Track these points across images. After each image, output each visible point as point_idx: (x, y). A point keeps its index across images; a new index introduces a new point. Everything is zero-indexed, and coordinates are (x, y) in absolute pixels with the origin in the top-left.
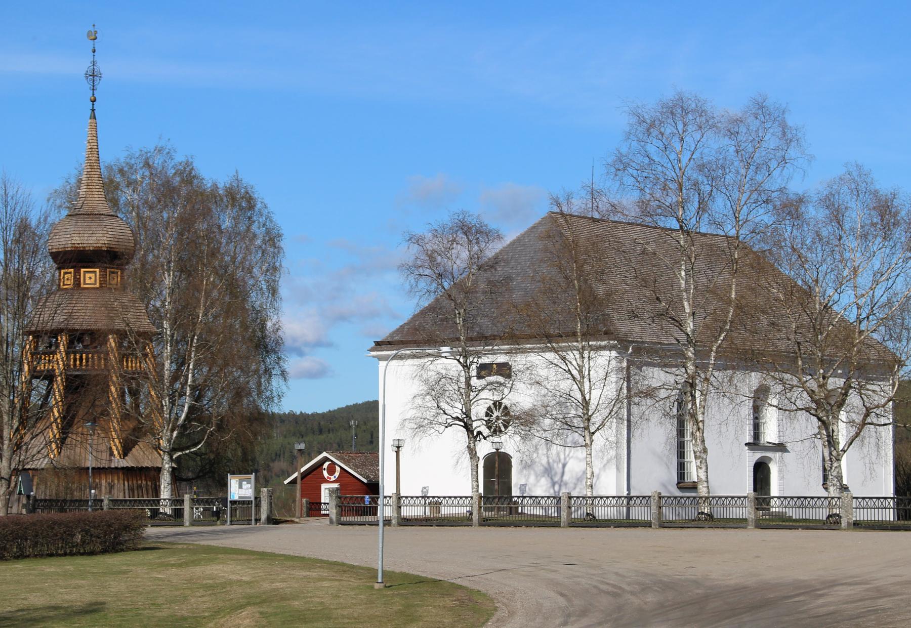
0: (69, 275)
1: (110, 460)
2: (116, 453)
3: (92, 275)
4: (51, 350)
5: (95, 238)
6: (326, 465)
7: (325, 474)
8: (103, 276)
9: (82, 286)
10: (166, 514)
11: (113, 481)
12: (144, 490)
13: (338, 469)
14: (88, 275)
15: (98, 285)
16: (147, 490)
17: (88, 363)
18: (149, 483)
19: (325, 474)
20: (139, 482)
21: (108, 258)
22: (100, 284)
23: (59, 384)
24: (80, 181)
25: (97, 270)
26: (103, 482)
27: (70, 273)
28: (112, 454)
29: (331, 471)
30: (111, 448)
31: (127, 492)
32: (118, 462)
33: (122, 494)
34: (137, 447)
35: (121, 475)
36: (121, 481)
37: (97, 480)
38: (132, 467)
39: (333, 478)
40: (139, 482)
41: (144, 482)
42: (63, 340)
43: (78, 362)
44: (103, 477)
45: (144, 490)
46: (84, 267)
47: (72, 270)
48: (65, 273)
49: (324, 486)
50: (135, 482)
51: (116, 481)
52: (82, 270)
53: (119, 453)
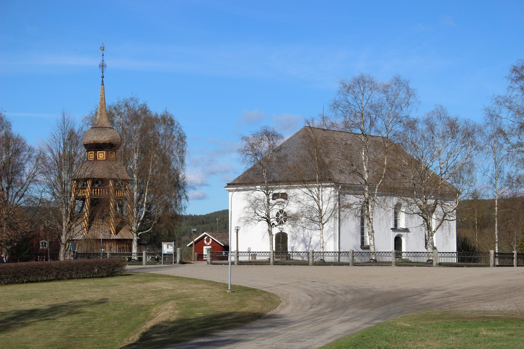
1: (110, 236)
2: (113, 232)
3: (102, 154)
4: (84, 187)
5: (104, 138)
6: (205, 238)
7: (205, 242)
8: (107, 155)
13: (211, 240)
14: (100, 154)
15: (105, 159)
17: (100, 193)
19: (205, 242)
21: (109, 147)
23: (87, 202)
26: (107, 245)
28: (111, 233)
29: (208, 241)
32: (114, 237)
39: (208, 244)
42: (89, 183)
44: (107, 243)
52: (98, 152)
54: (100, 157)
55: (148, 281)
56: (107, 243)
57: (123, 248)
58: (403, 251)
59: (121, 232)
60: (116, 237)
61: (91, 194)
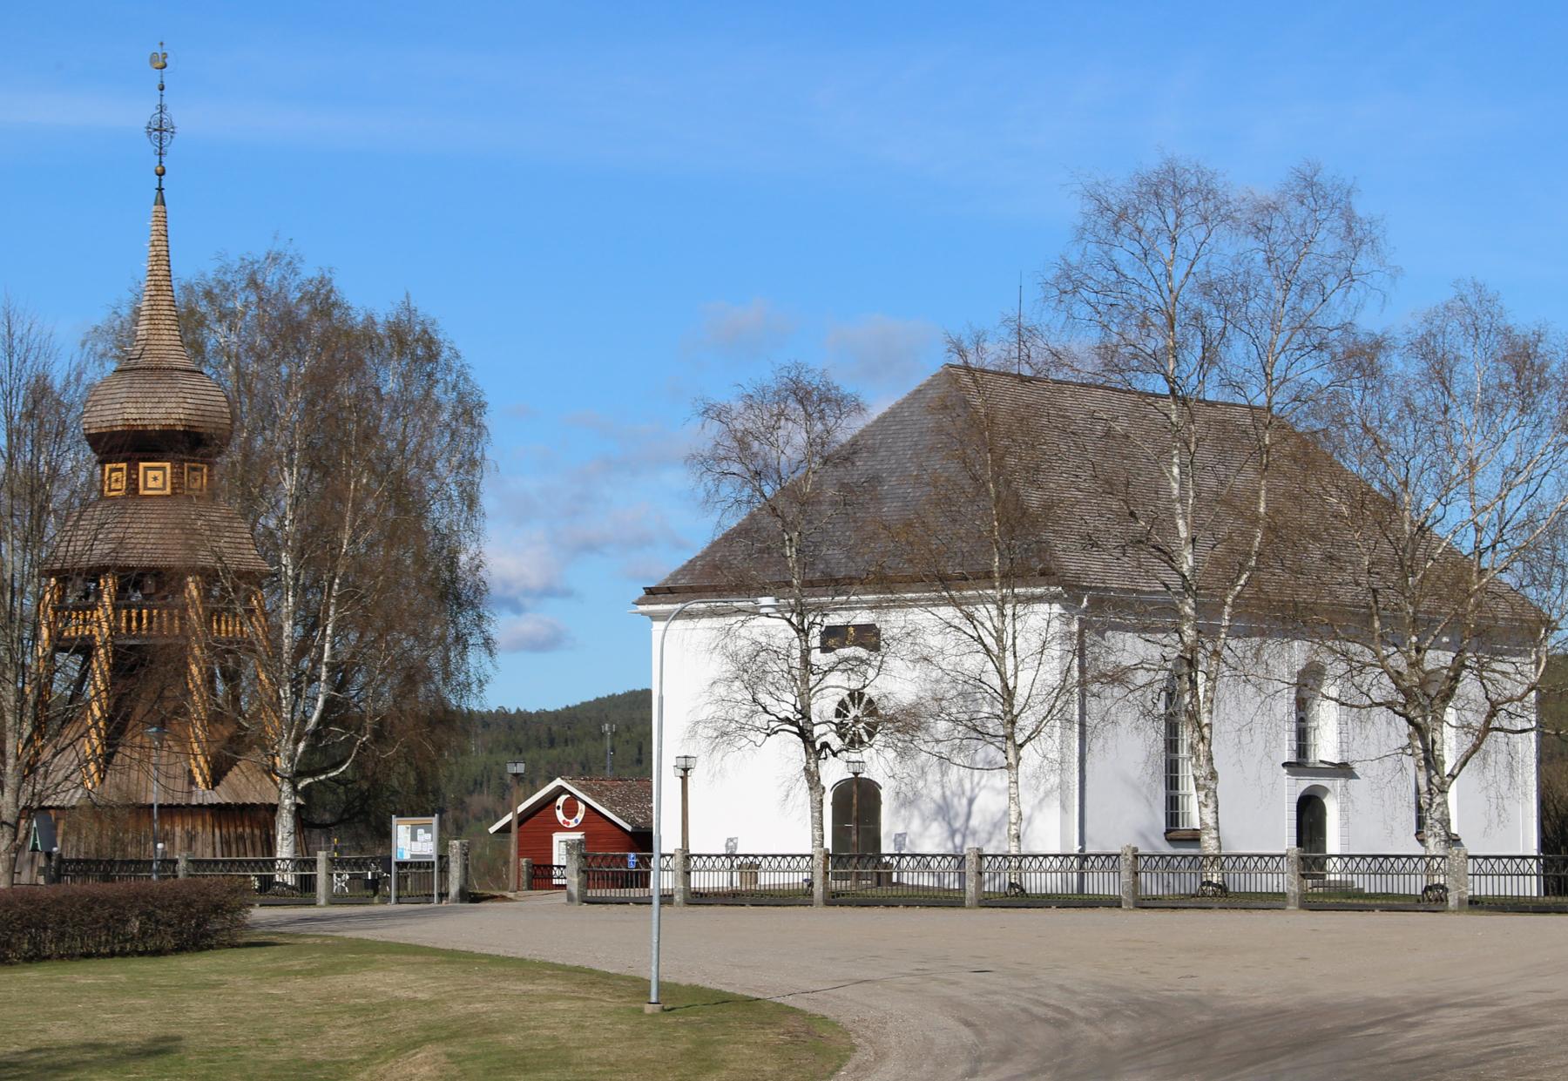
0: (119, 474)
1: (190, 793)
2: (199, 779)
3: (159, 473)
4: (88, 602)
5: (163, 409)
6: (561, 801)
7: (560, 815)
8: (177, 475)
9: (141, 492)
10: (285, 885)
11: (194, 828)
12: (248, 843)
13: (582, 807)
14: (151, 474)
15: (168, 491)
16: (253, 844)
18: (257, 832)
19: (560, 815)
20: (240, 830)
21: (186, 444)
22: (173, 489)
23: (101, 661)
25: (168, 465)
26: (178, 830)
27: (121, 470)
28: (192, 781)
29: (570, 811)
30: (190, 771)
31: (218, 846)
32: (204, 795)
33: (209, 850)
34: (235, 769)
35: (208, 818)
36: (209, 829)
37: (167, 827)
38: (228, 804)
39: (573, 824)
40: (240, 830)
41: (248, 830)
42: (108, 585)
43: (134, 624)
45: (248, 843)
46: (144, 460)
47: (124, 465)
48: (113, 470)
49: (558, 837)
50: (232, 830)
51: (200, 829)
52: (142, 465)
53: (204, 780)
56: (178, 820)
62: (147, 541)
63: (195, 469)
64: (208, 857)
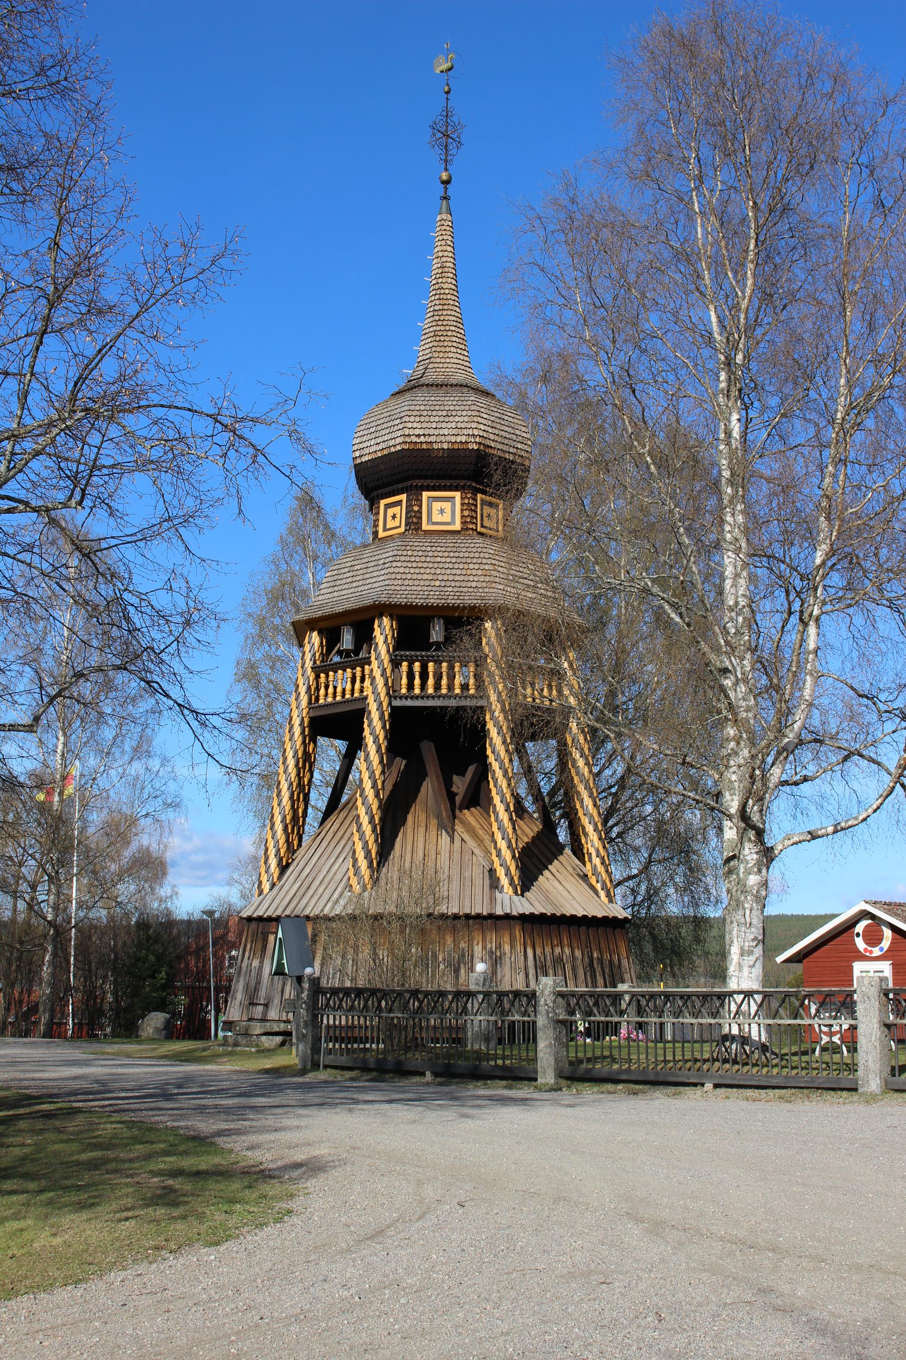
0: (396, 510)
1: (493, 900)
2: (504, 881)
3: (447, 506)
4: (356, 658)
5: (451, 426)
6: (860, 927)
7: (860, 944)
8: (469, 507)
9: (425, 526)
10: (744, 1040)
11: (499, 946)
12: (568, 968)
13: (888, 933)
14: (437, 506)
15: (457, 526)
16: (574, 969)
17: (447, 683)
18: (578, 953)
19: (860, 944)
20: (558, 950)
21: (474, 471)
22: (463, 523)
23: (374, 730)
24: (226, 1002)
25: (457, 495)
26: (478, 949)
27: (399, 503)
28: (495, 884)
29: (873, 938)
30: (492, 872)
31: (532, 971)
32: (510, 902)
33: (521, 977)
34: (546, 872)
35: (518, 933)
36: (519, 948)
37: (463, 945)
38: (543, 915)
39: (876, 952)
40: (558, 950)
41: (567, 951)
42: (383, 632)
43: (417, 681)
44: (477, 936)
45: (568, 968)
46: (428, 489)
47: (403, 497)
48: (388, 506)
49: (858, 967)
50: (548, 950)
51: (507, 948)
52: (425, 494)
53: (512, 882)
54: (436, 517)
55: (189, 1051)
56: (477, 936)
57: (558, 962)
58: (733, 985)
59: (545, 880)
60: (530, 904)
61: (392, 692)
62: (425, 580)
63: (491, 504)
64: (477, 910)
